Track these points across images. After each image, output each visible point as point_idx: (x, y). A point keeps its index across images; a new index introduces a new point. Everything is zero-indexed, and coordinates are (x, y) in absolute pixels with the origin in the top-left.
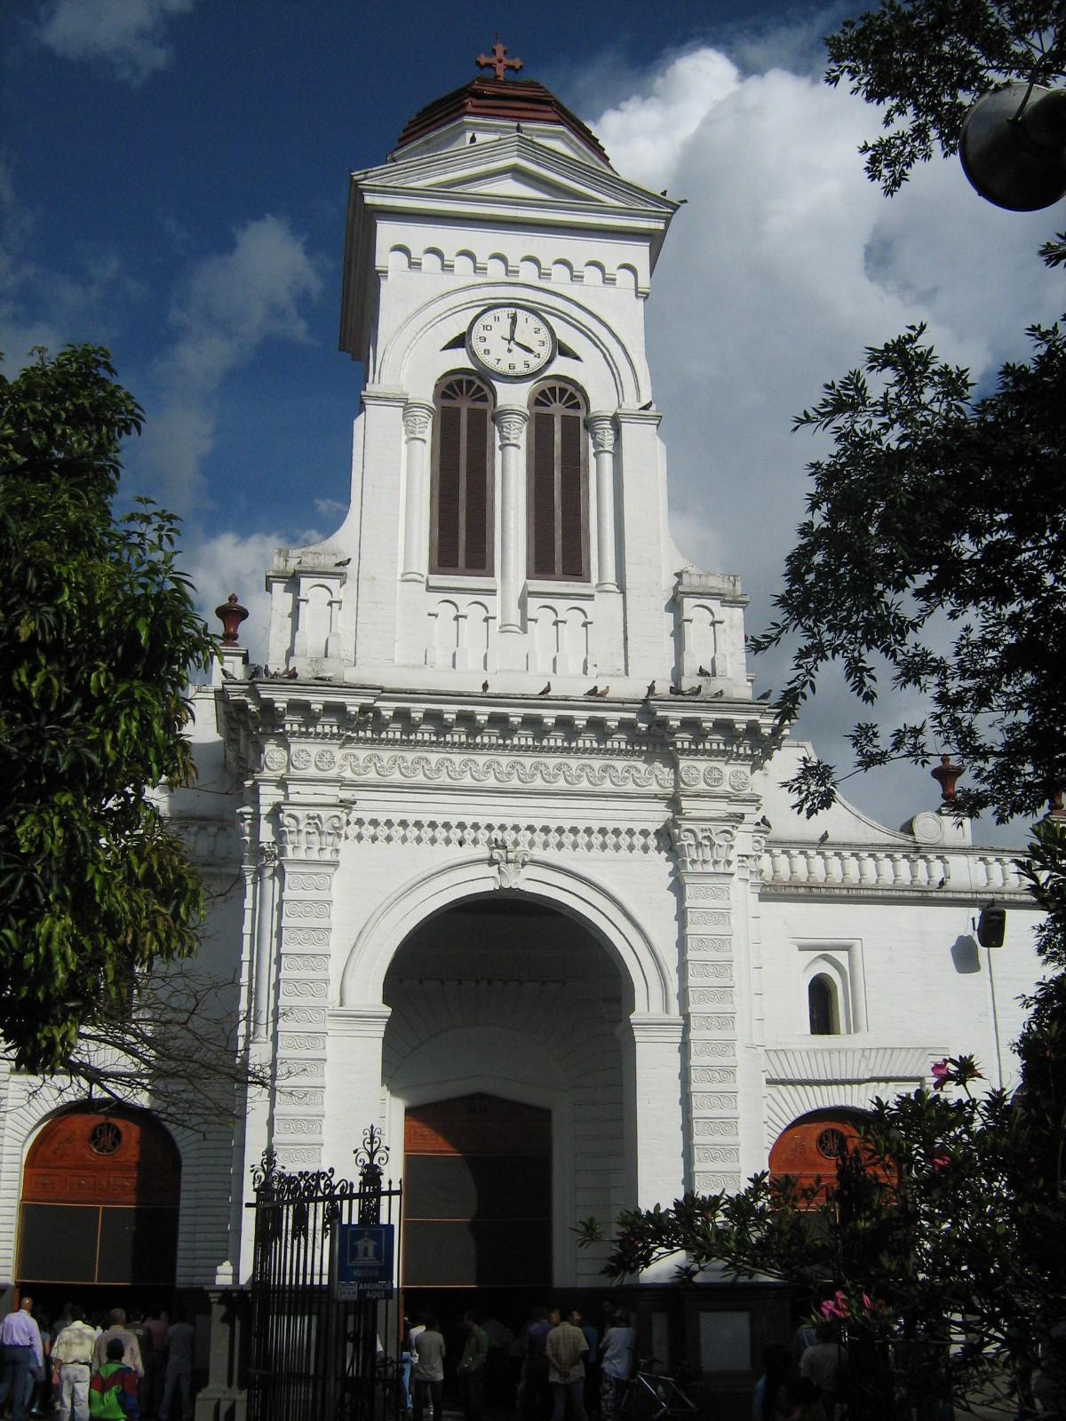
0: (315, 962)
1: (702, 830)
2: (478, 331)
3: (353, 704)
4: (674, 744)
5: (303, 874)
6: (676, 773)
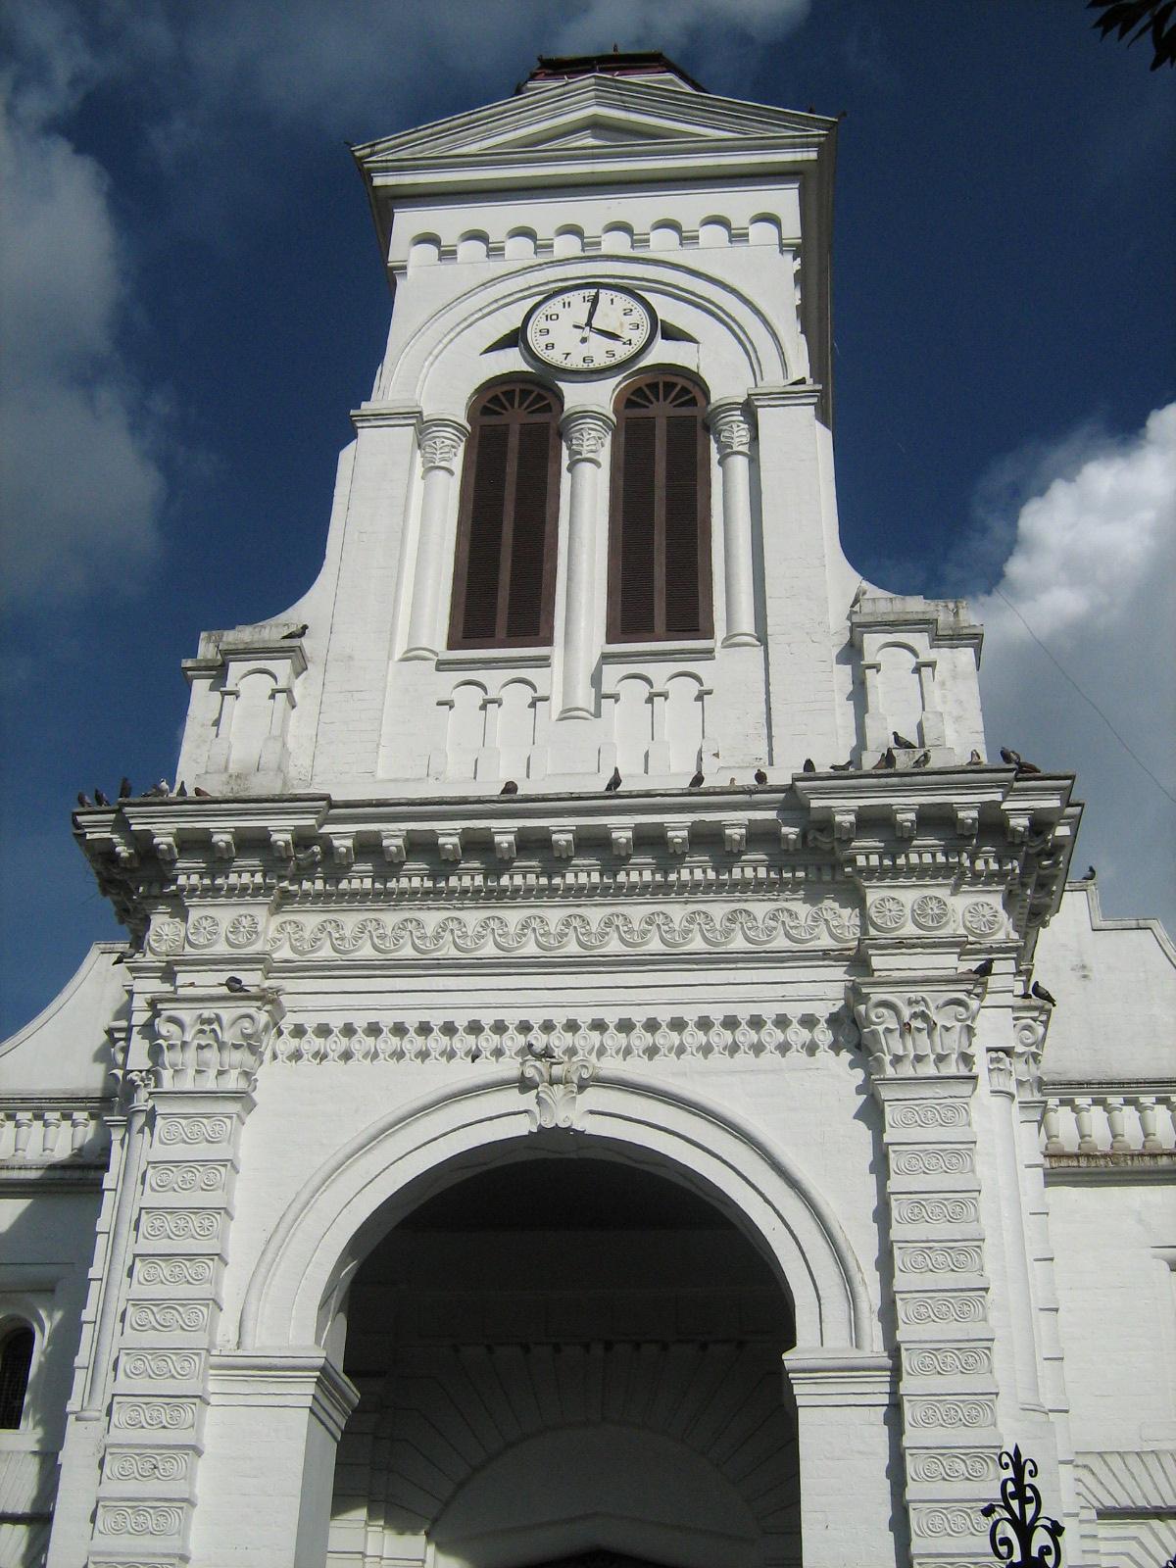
0: (190, 1268)
1: (910, 1003)
2: (538, 322)
3: (281, 829)
4: (852, 861)
5: (186, 1116)
6: (864, 915)
